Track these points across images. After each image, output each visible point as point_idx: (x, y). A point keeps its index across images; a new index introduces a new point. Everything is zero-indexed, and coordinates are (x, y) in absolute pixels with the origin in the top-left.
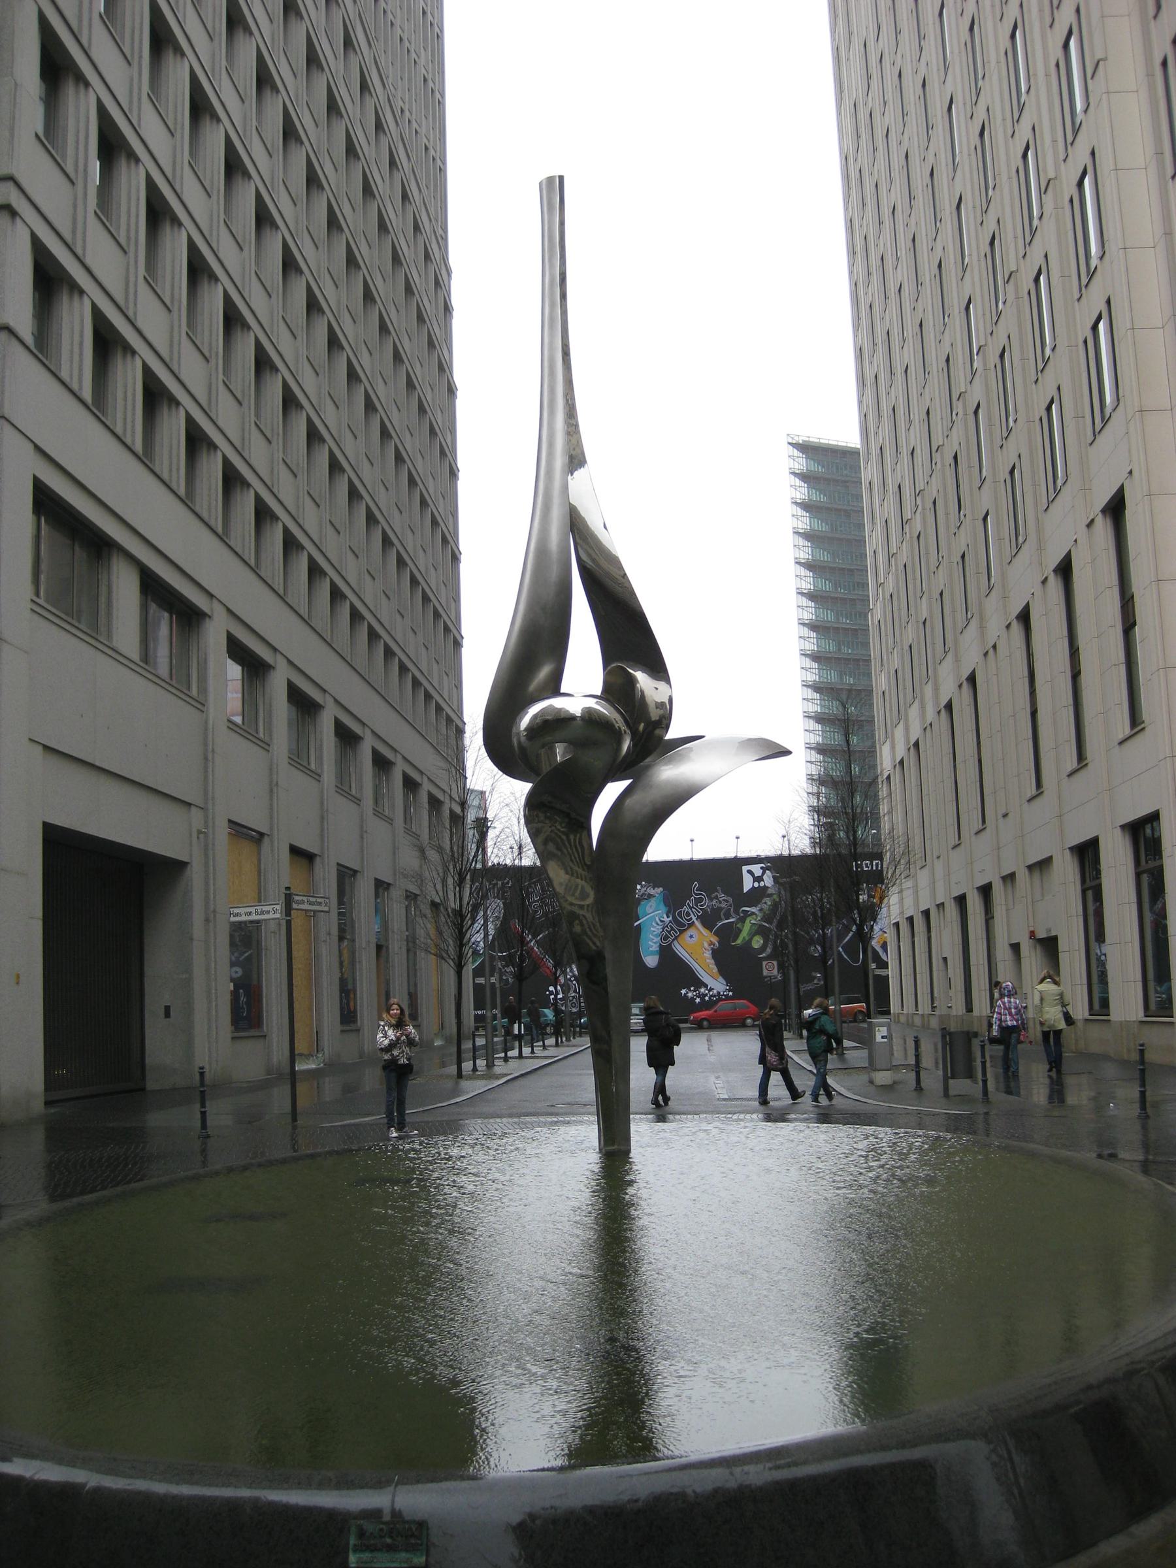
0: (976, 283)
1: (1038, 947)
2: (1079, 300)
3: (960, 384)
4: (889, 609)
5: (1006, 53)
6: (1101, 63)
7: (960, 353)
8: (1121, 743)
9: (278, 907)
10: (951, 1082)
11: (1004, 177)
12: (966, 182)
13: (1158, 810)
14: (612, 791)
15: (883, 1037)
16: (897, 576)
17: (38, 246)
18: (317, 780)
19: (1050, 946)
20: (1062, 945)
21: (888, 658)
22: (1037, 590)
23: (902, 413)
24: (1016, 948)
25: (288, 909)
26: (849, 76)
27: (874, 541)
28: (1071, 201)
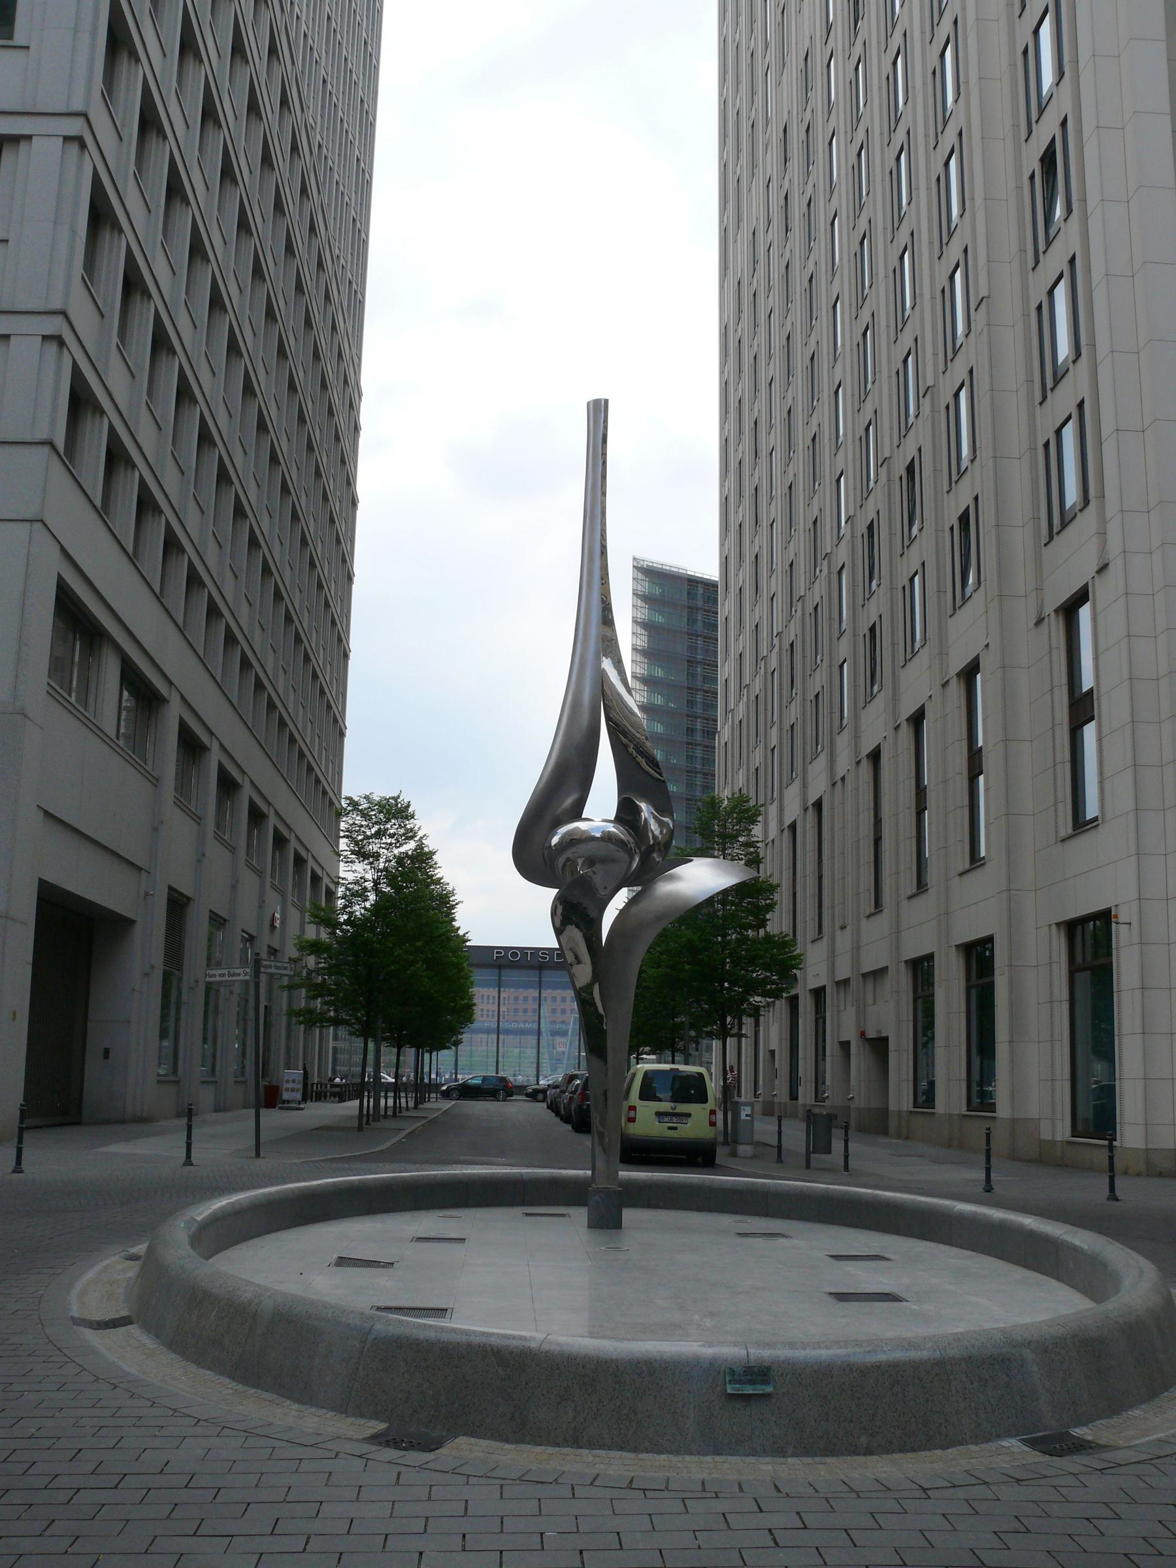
0: (847, 459)
1: (867, 1046)
4: (737, 734)
7: (828, 519)
8: (961, 875)
9: (248, 970)
10: (812, 1155)
11: (885, 374)
13: (993, 935)
14: (622, 898)
15: (746, 1115)
17: (76, 371)
18: (231, 851)
19: (879, 1046)
21: (733, 777)
22: (890, 733)
23: (765, 561)
24: (845, 1046)
25: (257, 973)
26: (735, 256)
27: (726, 670)
28: (898, 372)
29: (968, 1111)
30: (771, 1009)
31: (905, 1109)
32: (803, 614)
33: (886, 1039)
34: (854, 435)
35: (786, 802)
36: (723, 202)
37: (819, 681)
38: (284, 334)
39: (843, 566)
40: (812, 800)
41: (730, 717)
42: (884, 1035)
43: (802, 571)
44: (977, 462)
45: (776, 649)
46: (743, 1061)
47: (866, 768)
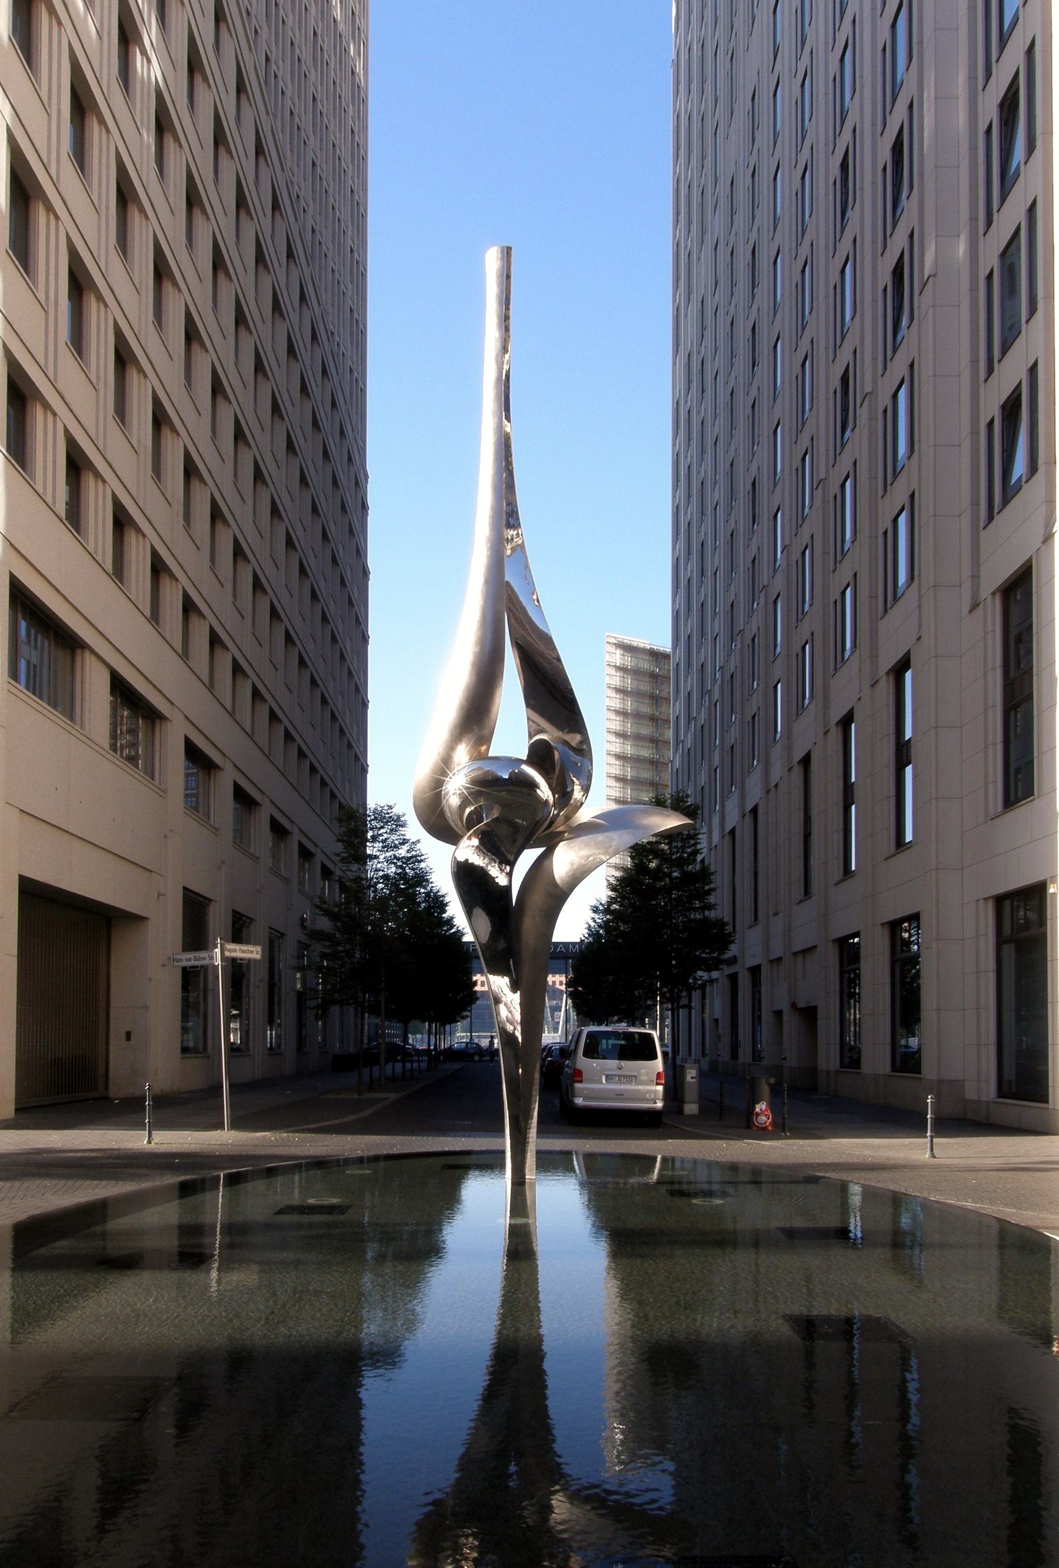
2: (834, 571)
3: (764, 578)
4: (699, 741)
5: (797, 377)
6: (930, 279)
12: (784, 409)
16: (683, 756)
19: (809, 1014)
20: (820, 1014)
24: (778, 1014)
26: (686, 330)
29: (892, 1071)
30: (715, 985)
31: (833, 1069)
32: (742, 646)
33: (815, 1008)
34: (791, 466)
35: (727, 811)
36: (675, 285)
37: (755, 703)
38: (292, 334)
39: (779, 594)
40: (749, 807)
41: (707, 700)
42: (812, 1004)
43: (742, 609)
44: (857, 543)
45: (719, 682)
46: (693, 1027)
47: (797, 773)
